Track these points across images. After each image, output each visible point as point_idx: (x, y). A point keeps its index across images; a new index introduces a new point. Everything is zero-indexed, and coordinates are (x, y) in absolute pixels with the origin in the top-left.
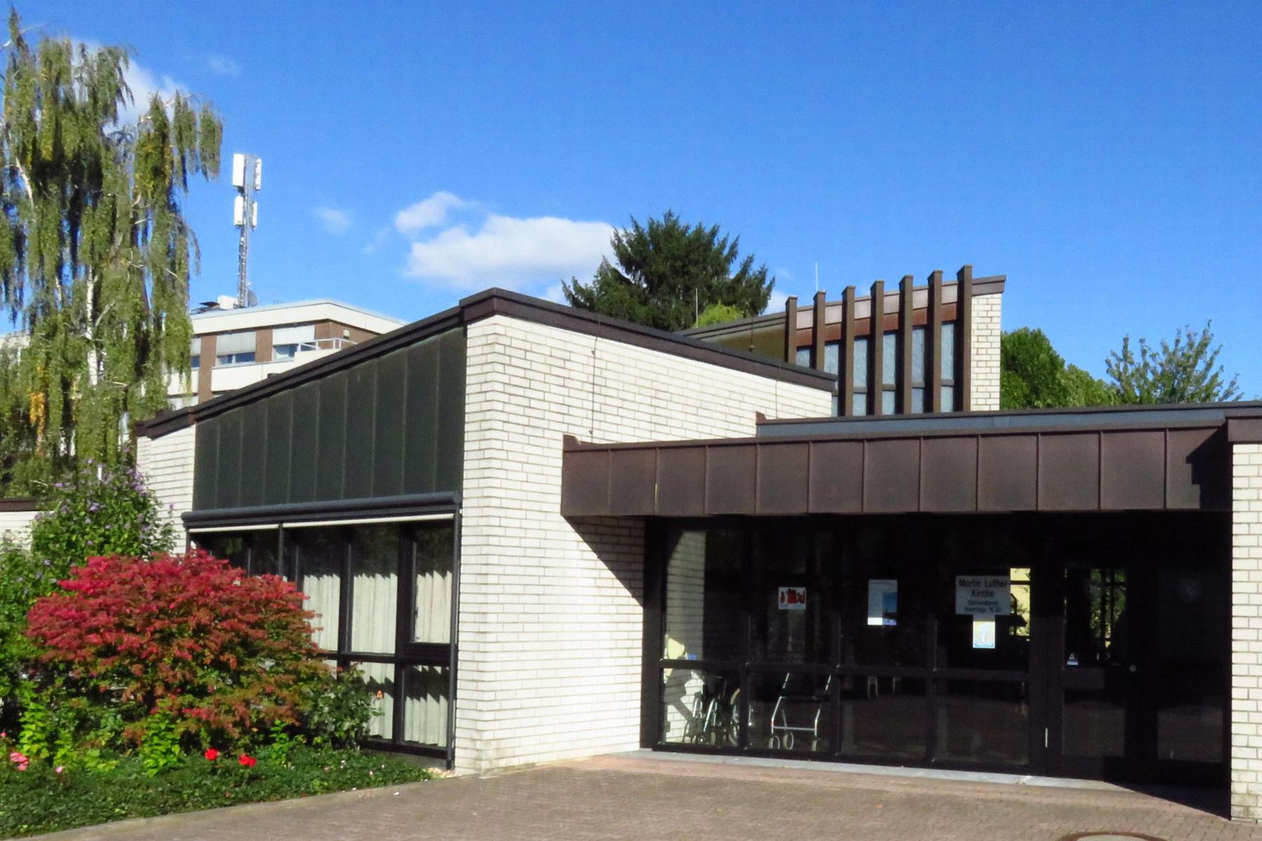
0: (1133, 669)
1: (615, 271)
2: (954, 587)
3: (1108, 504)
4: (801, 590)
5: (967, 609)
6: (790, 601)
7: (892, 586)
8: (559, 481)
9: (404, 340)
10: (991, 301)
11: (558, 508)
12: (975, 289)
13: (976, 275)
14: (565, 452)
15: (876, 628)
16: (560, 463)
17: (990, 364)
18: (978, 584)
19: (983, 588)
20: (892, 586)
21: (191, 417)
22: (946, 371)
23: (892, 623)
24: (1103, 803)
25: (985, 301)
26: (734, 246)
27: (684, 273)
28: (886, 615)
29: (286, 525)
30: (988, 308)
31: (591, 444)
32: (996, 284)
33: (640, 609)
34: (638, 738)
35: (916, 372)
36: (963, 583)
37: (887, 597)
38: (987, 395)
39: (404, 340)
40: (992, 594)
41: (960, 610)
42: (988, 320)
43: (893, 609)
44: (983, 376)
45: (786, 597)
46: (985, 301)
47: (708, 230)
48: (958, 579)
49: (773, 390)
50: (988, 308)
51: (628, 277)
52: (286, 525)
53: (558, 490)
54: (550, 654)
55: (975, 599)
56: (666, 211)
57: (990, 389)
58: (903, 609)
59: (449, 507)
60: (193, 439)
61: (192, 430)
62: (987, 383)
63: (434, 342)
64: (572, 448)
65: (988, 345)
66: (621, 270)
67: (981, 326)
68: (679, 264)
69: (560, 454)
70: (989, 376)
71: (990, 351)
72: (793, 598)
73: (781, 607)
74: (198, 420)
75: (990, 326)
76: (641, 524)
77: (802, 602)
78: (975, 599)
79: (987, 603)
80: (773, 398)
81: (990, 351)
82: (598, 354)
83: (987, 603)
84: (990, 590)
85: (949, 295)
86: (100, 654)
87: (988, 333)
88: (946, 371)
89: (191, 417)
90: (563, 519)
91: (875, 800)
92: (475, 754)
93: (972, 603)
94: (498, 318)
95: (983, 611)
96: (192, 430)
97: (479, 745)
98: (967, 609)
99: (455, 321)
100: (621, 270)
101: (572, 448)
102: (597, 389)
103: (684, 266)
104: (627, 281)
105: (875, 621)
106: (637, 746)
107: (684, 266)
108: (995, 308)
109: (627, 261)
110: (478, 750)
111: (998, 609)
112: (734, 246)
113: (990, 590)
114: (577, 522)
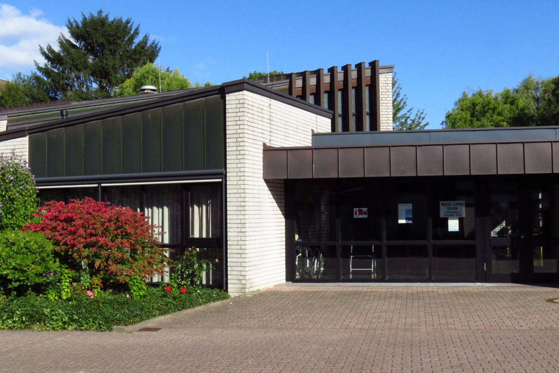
0: (522, 237)
1: (69, 41)
2: (439, 205)
3: (529, 171)
4: (365, 209)
5: (445, 215)
6: (360, 214)
7: (410, 206)
8: (262, 164)
9: (181, 100)
10: (387, 76)
11: (262, 176)
12: (381, 71)
13: (381, 64)
14: (264, 150)
15: (402, 225)
16: (262, 155)
17: (387, 105)
18: (450, 204)
19: (452, 206)
20: (410, 206)
21: (27, 132)
22: (366, 108)
23: (410, 222)
24: (518, 290)
25: (384, 76)
26: (137, 29)
27: (114, 43)
28: (406, 219)
29: (103, 185)
30: (386, 79)
31: (270, 147)
32: (390, 68)
33: (284, 220)
34: (285, 277)
35: (352, 109)
36: (443, 204)
37: (407, 211)
38: (387, 119)
39: (181, 100)
40: (456, 209)
41: (442, 215)
42: (386, 85)
43: (411, 216)
44: (385, 110)
45: (358, 212)
46: (384, 76)
47: (124, 20)
48: (441, 202)
49: (315, 119)
50: (386, 79)
51: (78, 45)
52: (103, 185)
53: (262, 168)
54: (259, 240)
55: (448, 211)
56: (98, 10)
57: (388, 116)
58: (416, 215)
59: (221, 176)
60: (27, 142)
61: (27, 138)
62: (387, 113)
63: (202, 101)
64: (267, 150)
65: (386, 96)
66: (73, 41)
67: (383, 88)
68: (112, 39)
69: (262, 151)
70: (388, 110)
71: (387, 99)
72: (361, 213)
73: (355, 217)
74: (29, 134)
75: (387, 88)
76: (283, 182)
77: (366, 214)
78: (448, 211)
79: (454, 212)
80: (315, 123)
81: (387, 99)
82: (272, 106)
83: (454, 212)
84: (456, 207)
85: (367, 73)
86: (85, 247)
87: (386, 90)
88: (366, 108)
89: (27, 132)
90: (263, 181)
91: (396, 296)
92: (241, 286)
93: (447, 212)
94: (245, 92)
95: (453, 216)
96: (27, 138)
97: (243, 282)
98: (445, 215)
99: (217, 92)
100: (73, 41)
101: (267, 150)
102: (272, 123)
103: (115, 40)
104: (75, 46)
105: (402, 221)
106: (284, 281)
107: (115, 40)
108: (389, 79)
109: (76, 35)
110: (243, 284)
111: (460, 215)
112: (137, 29)
113: (456, 207)
114: (267, 181)
